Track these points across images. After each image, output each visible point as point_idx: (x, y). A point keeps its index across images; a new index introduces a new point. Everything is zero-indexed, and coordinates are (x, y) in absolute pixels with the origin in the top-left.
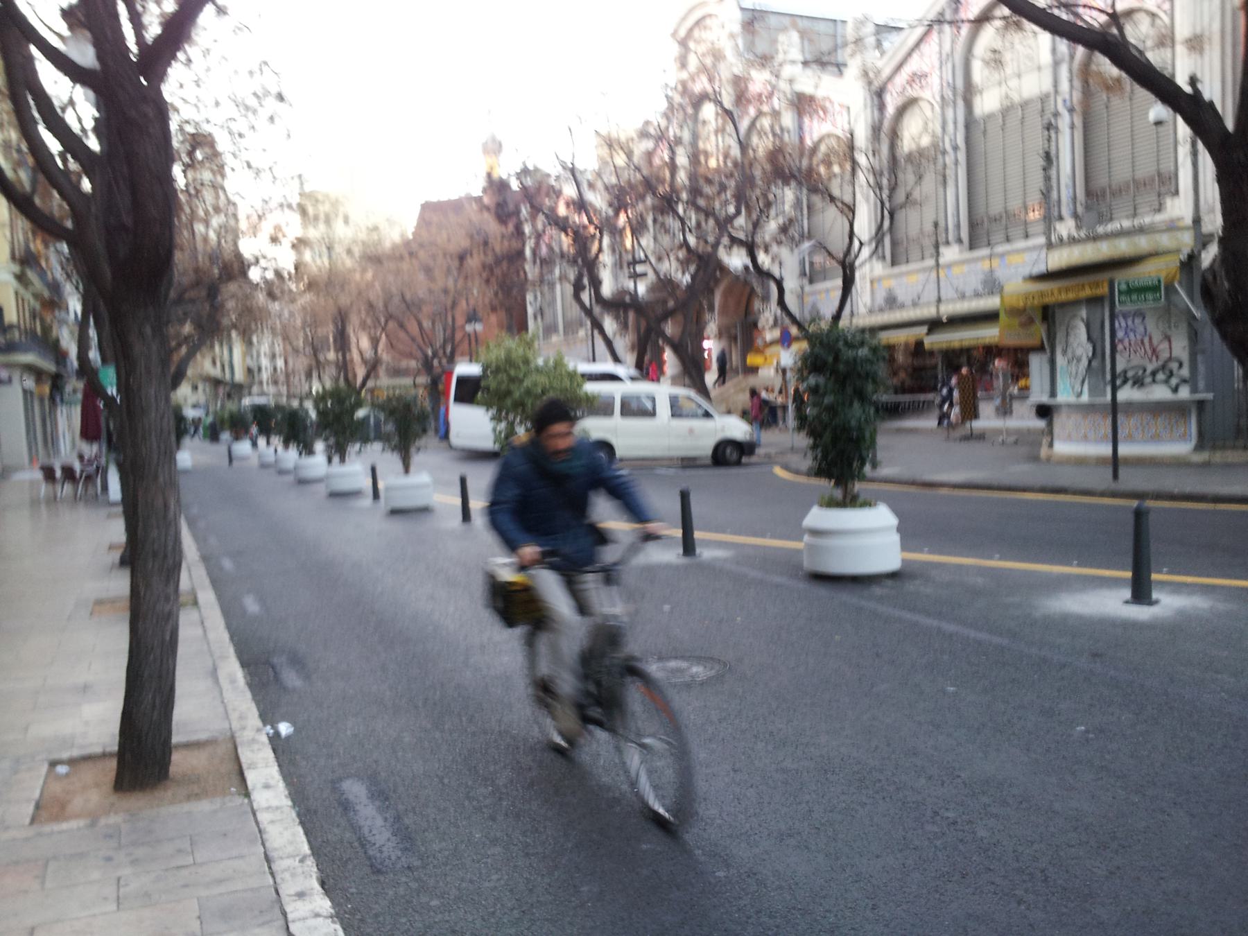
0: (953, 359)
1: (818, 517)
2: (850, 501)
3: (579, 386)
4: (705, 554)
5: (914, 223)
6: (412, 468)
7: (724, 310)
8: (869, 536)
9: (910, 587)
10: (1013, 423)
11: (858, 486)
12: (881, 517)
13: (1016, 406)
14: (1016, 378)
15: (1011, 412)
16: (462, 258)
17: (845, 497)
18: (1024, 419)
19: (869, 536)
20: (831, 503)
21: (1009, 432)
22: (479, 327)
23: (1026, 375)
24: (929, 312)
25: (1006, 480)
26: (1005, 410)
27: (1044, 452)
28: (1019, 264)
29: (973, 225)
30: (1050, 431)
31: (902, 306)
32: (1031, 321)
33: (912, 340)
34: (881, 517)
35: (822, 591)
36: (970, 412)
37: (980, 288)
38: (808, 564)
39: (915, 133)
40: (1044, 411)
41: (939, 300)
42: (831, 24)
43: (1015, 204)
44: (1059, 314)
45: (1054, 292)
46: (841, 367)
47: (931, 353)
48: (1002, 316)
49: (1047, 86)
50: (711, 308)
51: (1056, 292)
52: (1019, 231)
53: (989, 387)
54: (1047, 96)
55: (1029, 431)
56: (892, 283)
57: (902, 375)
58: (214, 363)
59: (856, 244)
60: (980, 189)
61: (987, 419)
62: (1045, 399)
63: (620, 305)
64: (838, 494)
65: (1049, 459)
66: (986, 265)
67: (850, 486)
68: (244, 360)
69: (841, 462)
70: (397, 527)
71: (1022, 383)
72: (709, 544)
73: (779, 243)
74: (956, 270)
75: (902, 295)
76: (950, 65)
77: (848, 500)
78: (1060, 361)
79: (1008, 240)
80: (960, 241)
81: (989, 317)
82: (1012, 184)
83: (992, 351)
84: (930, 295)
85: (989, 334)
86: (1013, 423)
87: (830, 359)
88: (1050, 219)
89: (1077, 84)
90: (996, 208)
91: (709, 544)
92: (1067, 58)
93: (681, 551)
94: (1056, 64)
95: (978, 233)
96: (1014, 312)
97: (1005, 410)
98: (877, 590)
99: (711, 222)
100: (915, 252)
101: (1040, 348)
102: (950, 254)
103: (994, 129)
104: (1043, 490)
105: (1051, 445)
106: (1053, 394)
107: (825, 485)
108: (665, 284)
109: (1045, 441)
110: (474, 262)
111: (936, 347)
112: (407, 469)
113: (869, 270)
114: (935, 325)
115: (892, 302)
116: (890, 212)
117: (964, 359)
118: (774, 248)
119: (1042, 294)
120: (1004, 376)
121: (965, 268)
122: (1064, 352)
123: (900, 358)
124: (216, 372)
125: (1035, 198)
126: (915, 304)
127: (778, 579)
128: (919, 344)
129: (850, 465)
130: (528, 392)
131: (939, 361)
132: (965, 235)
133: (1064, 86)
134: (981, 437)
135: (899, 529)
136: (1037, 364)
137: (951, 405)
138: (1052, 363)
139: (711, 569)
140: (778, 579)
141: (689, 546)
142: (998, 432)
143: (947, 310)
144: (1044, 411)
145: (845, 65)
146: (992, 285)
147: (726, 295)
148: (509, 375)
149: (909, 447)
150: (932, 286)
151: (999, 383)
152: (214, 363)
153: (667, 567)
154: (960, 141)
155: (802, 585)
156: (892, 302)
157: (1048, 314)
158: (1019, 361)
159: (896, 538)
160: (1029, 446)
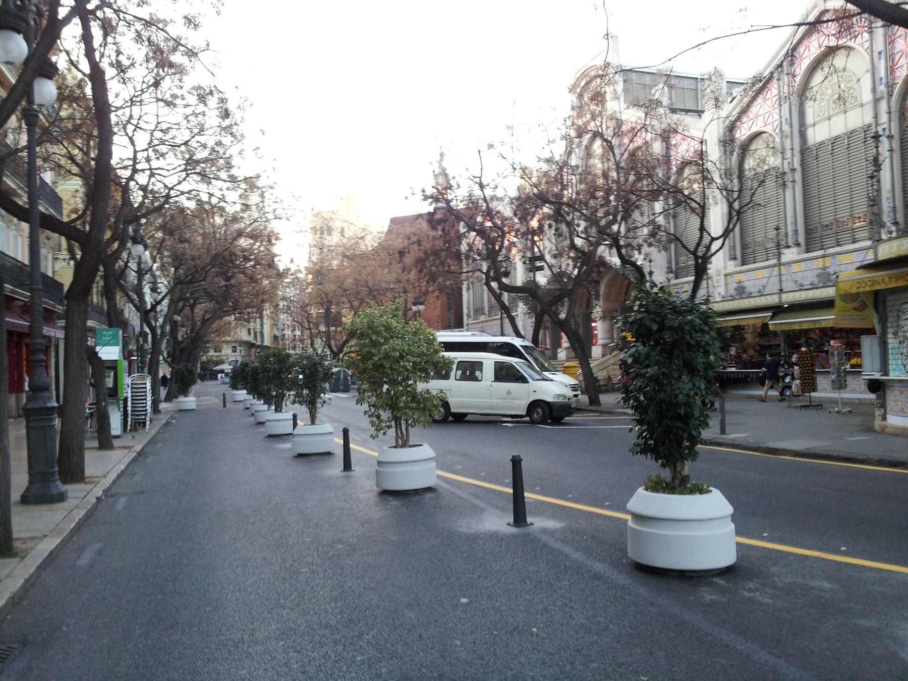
0: (794, 338)
1: (644, 500)
2: (678, 485)
3: (436, 352)
4: (537, 522)
5: (761, 225)
6: (317, 421)
7: (607, 300)
8: (701, 527)
9: (749, 590)
10: (846, 395)
11: (688, 468)
12: (714, 504)
13: (850, 379)
14: (849, 357)
15: (846, 386)
16: (402, 253)
17: (674, 478)
18: (856, 391)
19: (701, 527)
20: (657, 486)
21: (846, 403)
22: (421, 307)
23: (859, 355)
24: (773, 300)
25: (844, 451)
26: (840, 385)
27: (878, 423)
28: (848, 262)
29: (809, 232)
30: (883, 406)
31: (750, 296)
32: (864, 306)
33: (759, 323)
34: (714, 504)
35: (642, 589)
36: (809, 385)
37: (816, 280)
38: (635, 553)
39: (762, 159)
40: (875, 386)
41: (781, 290)
42: (693, 81)
43: (843, 215)
44: (890, 300)
45: (884, 280)
46: (668, 336)
47: (775, 334)
48: (839, 304)
49: (868, 118)
50: (597, 296)
51: (887, 280)
52: (847, 236)
53: (825, 364)
54: (869, 126)
55: (861, 402)
56: (742, 277)
57: (751, 352)
58: (249, 333)
59: (706, 240)
60: (814, 202)
61: (824, 390)
62: (877, 376)
63: (530, 291)
64: (666, 474)
65: (883, 430)
66: (819, 263)
67: (679, 465)
68: (272, 330)
69: (670, 443)
70: (300, 468)
71: (854, 361)
72: (544, 509)
73: (650, 245)
74: (795, 268)
75: (750, 287)
76: (787, 105)
77: (677, 482)
78: (892, 342)
79: (838, 244)
80: (798, 245)
81: (826, 305)
82: (844, 198)
83: (828, 333)
84: (773, 287)
85: (827, 318)
86: (846, 395)
87: (655, 327)
88: (876, 222)
89: (895, 116)
90: (827, 219)
91: (544, 509)
92: (885, 95)
93: (512, 520)
94: (876, 101)
95: (812, 238)
96: (848, 297)
97: (840, 385)
98: (708, 595)
99: (594, 229)
100: (761, 255)
101: (871, 331)
102: (789, 255)
103: (824, 155)
104: (881, 463)
105: (884, 418)
106: (885, 370)
107: (652, 467)
108: (558, 277)
109: (878, 412)
110: (408, 260)
111: (779, 328)
112: (313, 422)
113: (719, 264)
114: (778, 310)
115: (741, 292)
116: (735, 216)
117: (802, 340)
118: (645, 249)
119: (874, 282)
120: (839, 354)
121: (802, 266)
122: (895, 334)
123: (749, 337)
124: (250, 339)
125: (862, 207)
126: (761, 294)
127: (599, 567)
128: (765, 325)
129: (680, 445)
130: (387, 356)
131: (781, 341)
132: (801, 239)
133: (884, 118)
134: (818, 406)
135: (734, 518)
136: (868, 344)
137: (793, 379)
138: (884, 344)
139: (532, 545)
140: (599, 567)
141: (520, 518)
142: (834, 402)
143: (788, 298)
144: (875, 386)
145: (703, 112)
146: (826, 279)
147: (609, 286)
148: (371, 340)
149: (749, 421)
150: (775, 280)
151: (834, 360)
152: (249, 333)
153: (495, 537)
154: (797, 164)
155: (622, 579)
156: (741, 292)
157: (879, 300)
158: (851, 339)
159: (732, 527)
160: (863, 417)
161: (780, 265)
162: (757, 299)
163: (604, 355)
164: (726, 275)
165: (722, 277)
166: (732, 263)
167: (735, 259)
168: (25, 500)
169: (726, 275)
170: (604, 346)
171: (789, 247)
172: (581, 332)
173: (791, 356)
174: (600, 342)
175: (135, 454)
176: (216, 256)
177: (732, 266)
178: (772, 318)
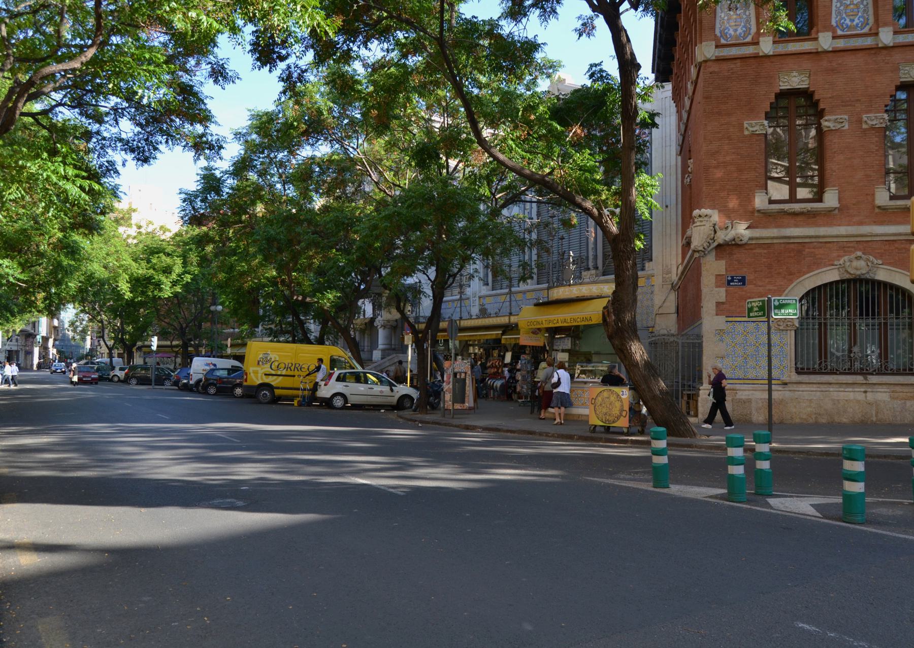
31: (489, 316)
75: (491, 309)
80: (596, 268)
121: (491, 300)
126: (497, 315)
161: (510, 293)
162: (476, 321)
163: (382, 359)
164: (480, 298)
165: (477, 299)
166: (485, 287)
167: (488, 284)
168: (754, 434)
169: (480, 298)
170: (383, 350)
171: (588, 269)
172: (357, 339)
173: (503, 357)
174: (380, 347)
175: (869, 377)
176: (195, 94)
177: (485, 291)
178: (503, 334)
